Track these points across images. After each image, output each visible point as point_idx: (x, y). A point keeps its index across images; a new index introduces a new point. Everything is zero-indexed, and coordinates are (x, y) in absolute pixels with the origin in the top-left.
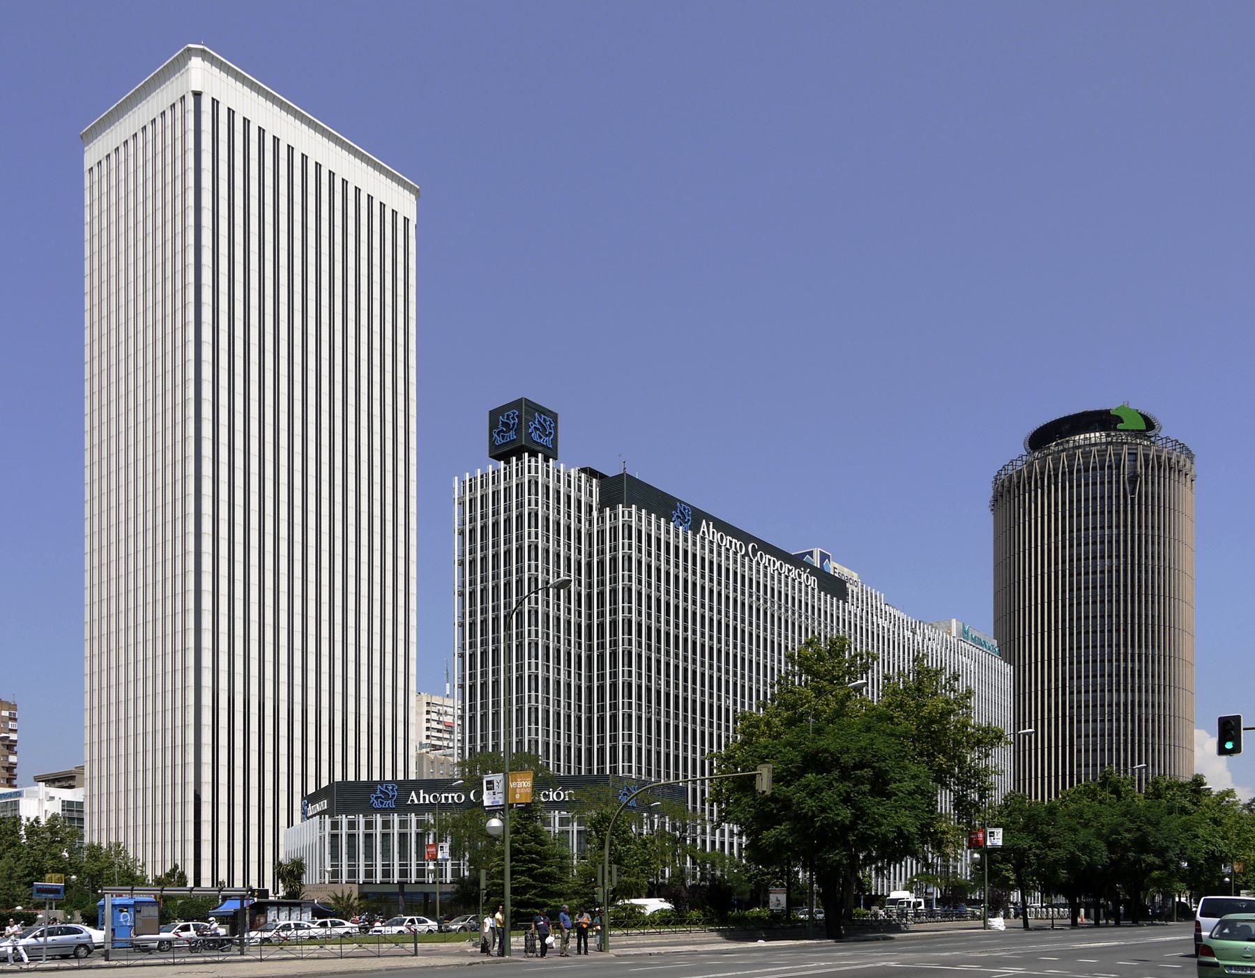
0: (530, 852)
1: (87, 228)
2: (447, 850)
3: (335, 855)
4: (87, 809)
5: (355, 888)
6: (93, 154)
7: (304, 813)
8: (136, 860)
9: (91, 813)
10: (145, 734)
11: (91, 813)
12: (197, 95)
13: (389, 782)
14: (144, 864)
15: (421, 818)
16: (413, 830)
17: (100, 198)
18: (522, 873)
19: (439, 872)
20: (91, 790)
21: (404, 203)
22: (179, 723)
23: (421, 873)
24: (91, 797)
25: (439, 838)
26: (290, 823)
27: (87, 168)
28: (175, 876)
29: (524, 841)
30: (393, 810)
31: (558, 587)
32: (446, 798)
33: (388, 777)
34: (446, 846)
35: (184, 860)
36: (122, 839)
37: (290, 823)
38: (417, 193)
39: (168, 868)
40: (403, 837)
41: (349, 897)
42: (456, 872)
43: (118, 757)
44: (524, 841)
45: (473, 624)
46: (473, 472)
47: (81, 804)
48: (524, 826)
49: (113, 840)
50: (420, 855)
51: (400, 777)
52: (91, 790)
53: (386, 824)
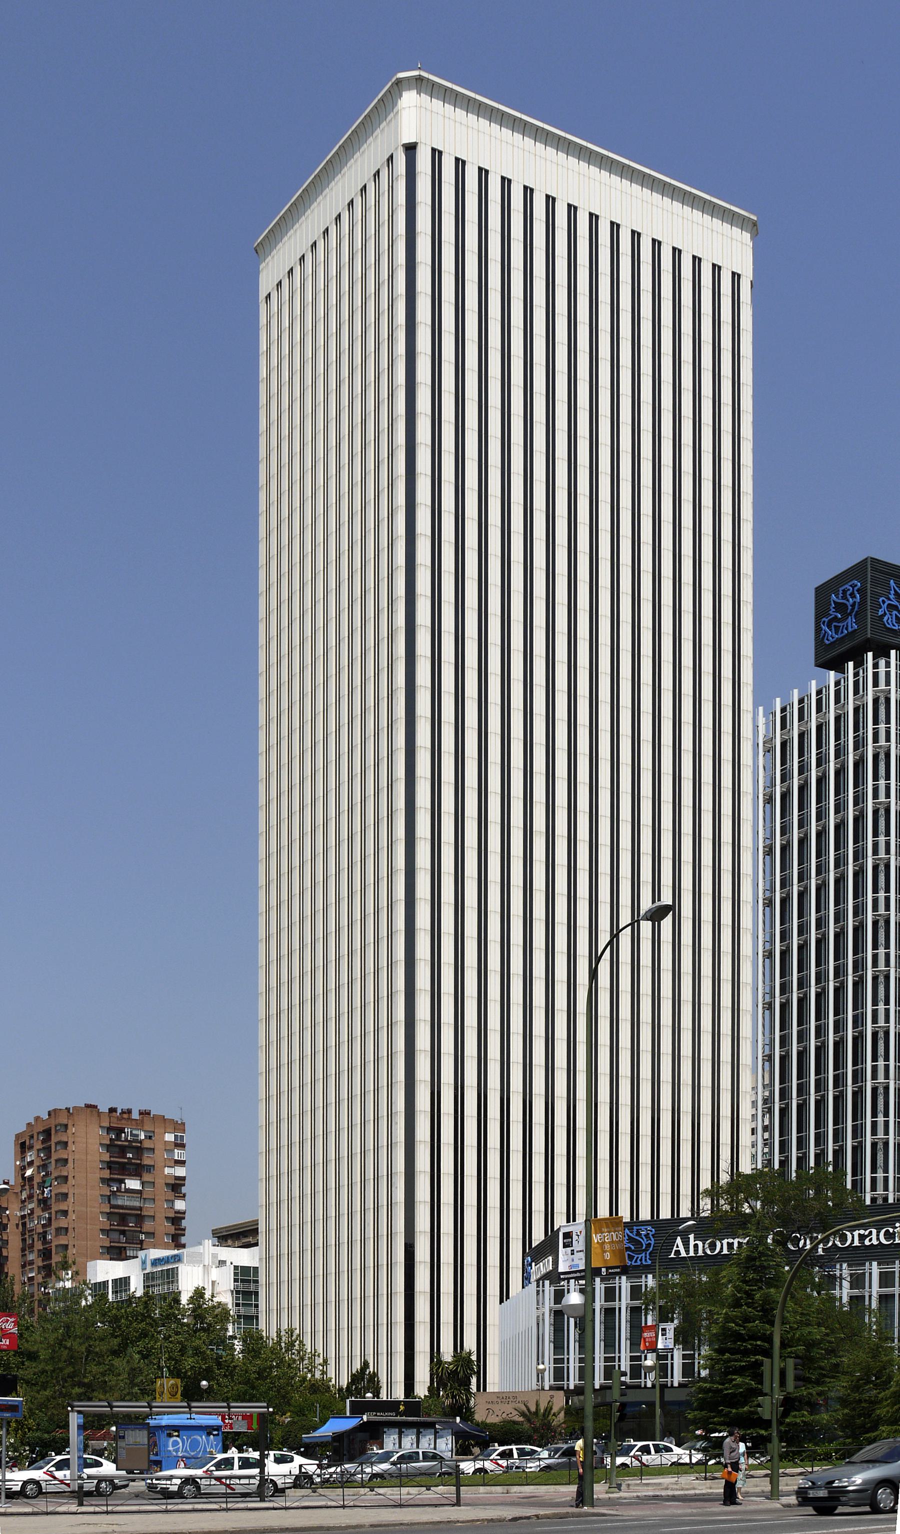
0: (753, 1337)
1: (262, 388)
2: (670, 1334)
3: (559, 1345)
4: (262, 1278)
5: (559, 1400)
6: (270, 272)
7: (526, 1279)
8: (314, 1355)
9: (268, 1285)
10: (338, 1159)
11: (268, 1285)
12: (411, 149)
13: (645, 1223)
14: (325, 1362)
15: (636, 1282)
16: (624, 1301)
17: (280, 337)
18: (739, 1371)
19: (663, 1369)
20: (268, 1250)
21: (729, 248)
22: (383, 1141)
23: (636, 1371)
24: (268, 1259)
25: (664, 1317)
26: (504, 1295)
27: (262, 295)
28: (364, 1379)
29: (747, 1319)
30: (647, 1269)
31: (657, 915)
32: (730, 1245)
33: (645, 1214)
34: (670, 1327)
35: (376, 1354)
36: (296, 1325)
37: (504, 1295)
38: (753, 228)
39: (357, 1366)
40: (610, 1314)
41: (548, 1410)
42: (688, 1369)
43: (290, 1199)
44: (747, 1319)
45: (785, 954)
46: (786, 696)
47: (256, 1269)
48: (749, 1295)
49: (285, 1326)
50: (634, 1343)
51: (665, 1213)
52: (268, 1250)
53: (610, 1294)
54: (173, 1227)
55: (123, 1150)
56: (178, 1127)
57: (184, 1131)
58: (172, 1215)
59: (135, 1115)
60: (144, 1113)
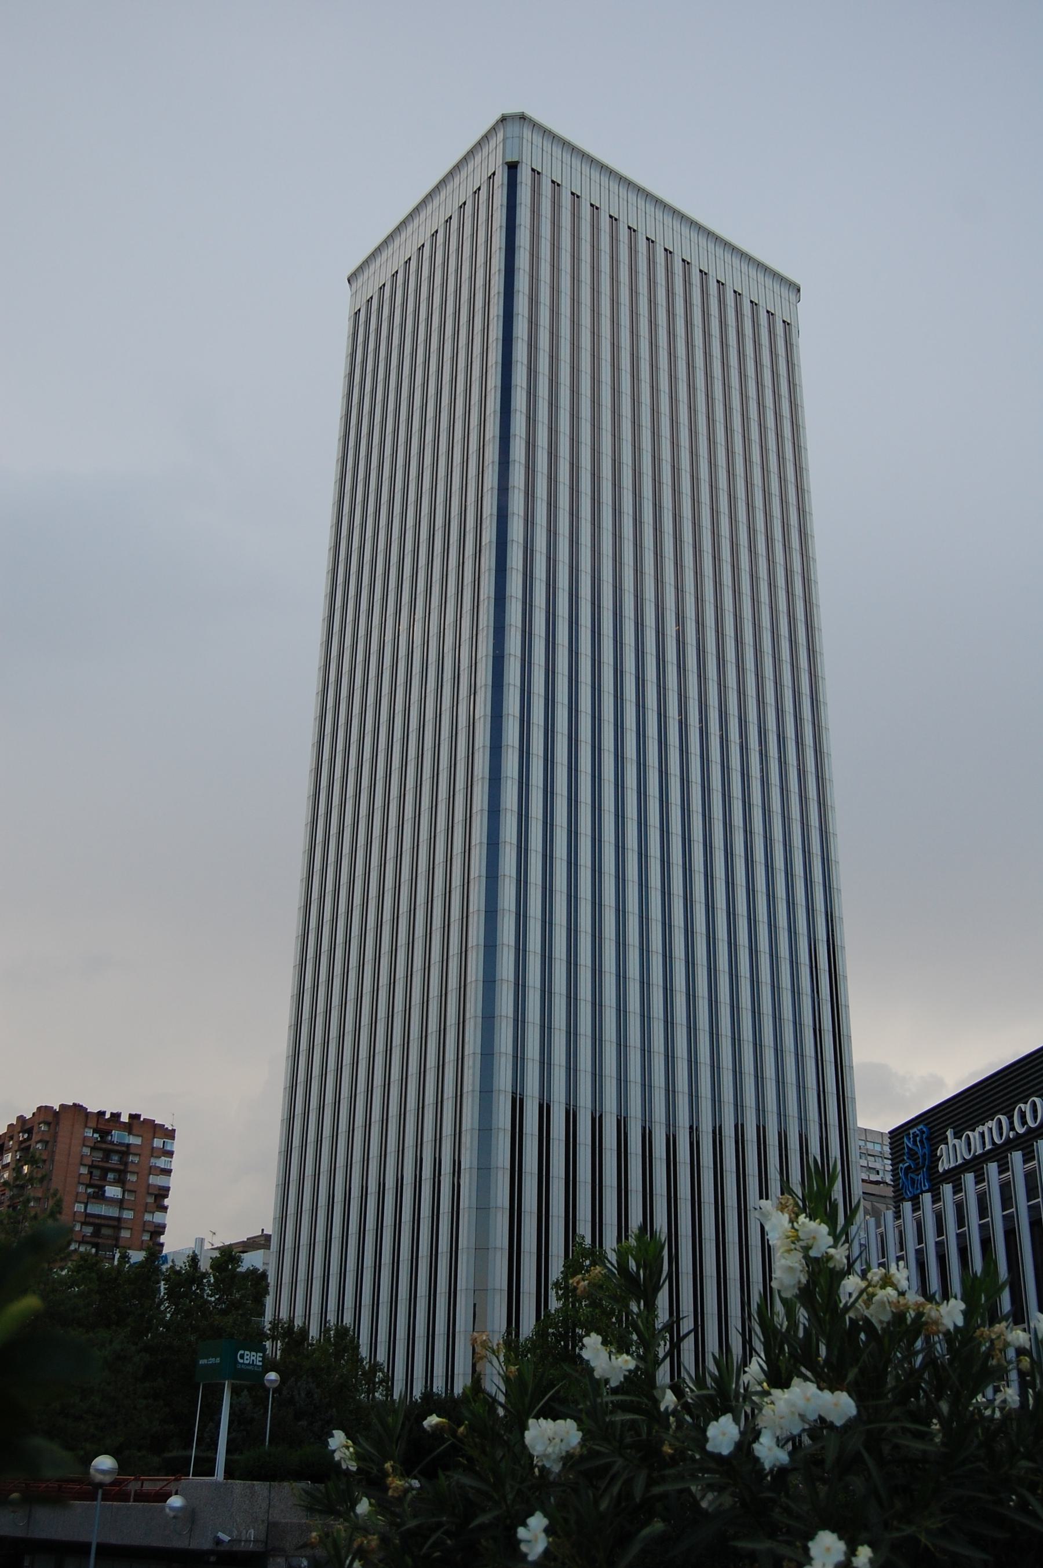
12: (512, 168)
54: (151, 1243)
55: (107, 1154)
56: (170, 1134)
57: (173, 1138)
58: (152, 1229)
59: (125, 1118)
60: (134, 1117)
